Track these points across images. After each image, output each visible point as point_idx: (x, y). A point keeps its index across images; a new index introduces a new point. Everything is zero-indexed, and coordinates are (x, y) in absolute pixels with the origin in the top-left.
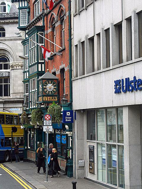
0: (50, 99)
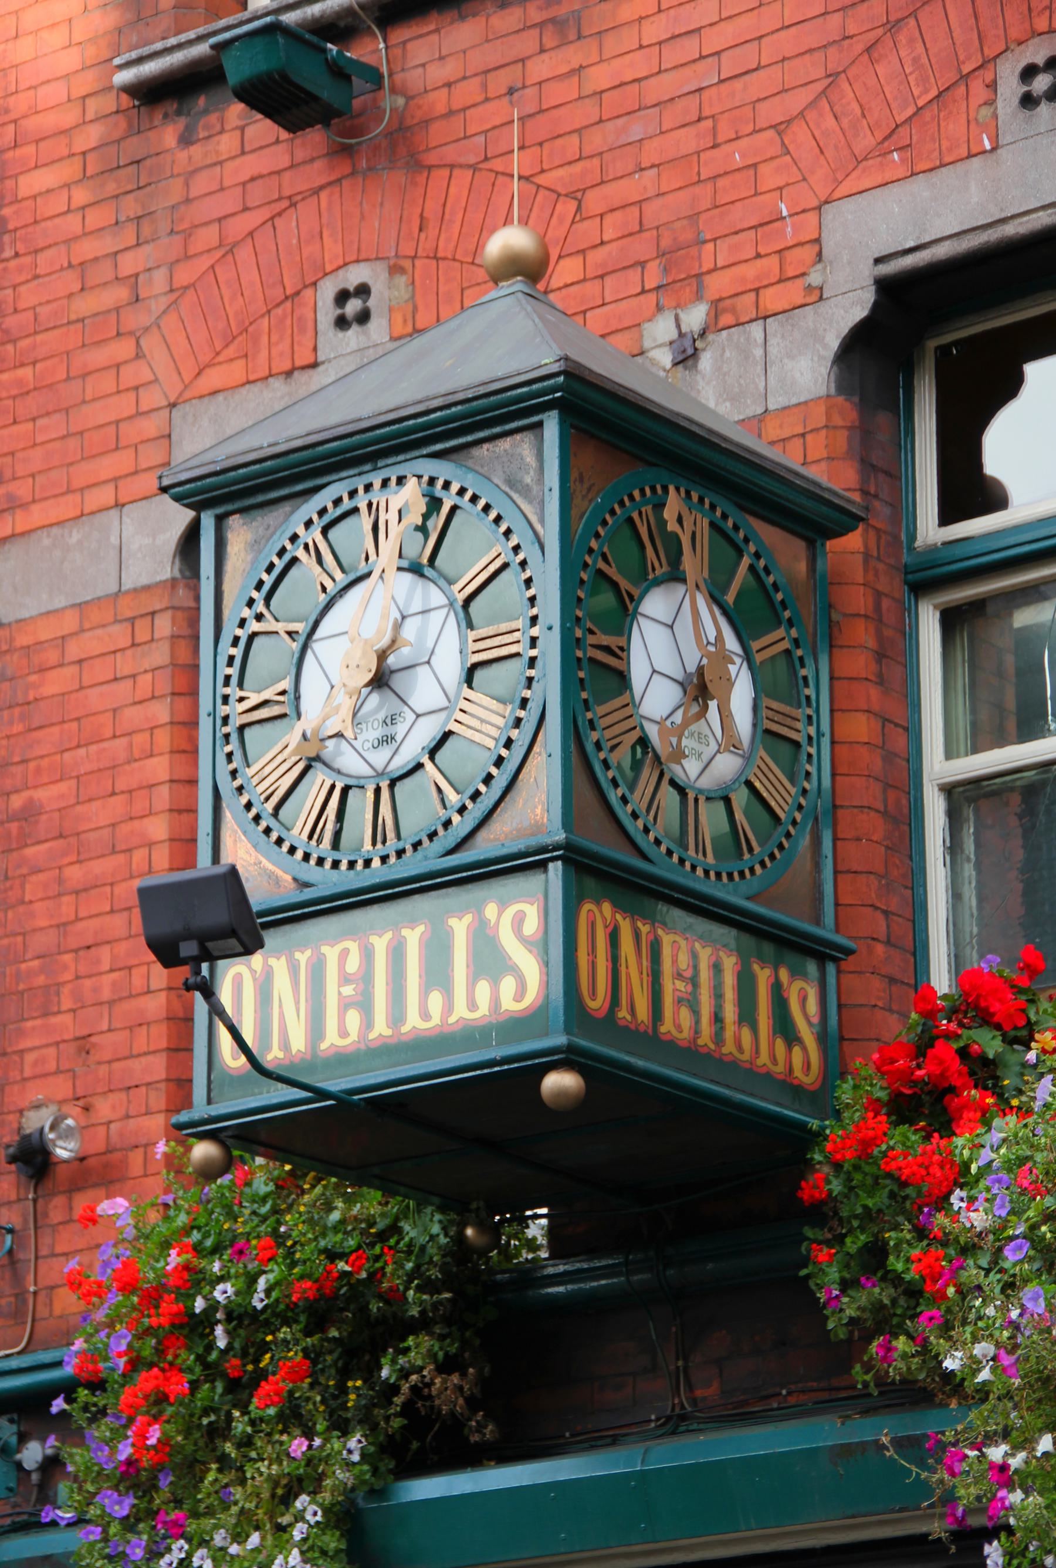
0: (365, 1006)
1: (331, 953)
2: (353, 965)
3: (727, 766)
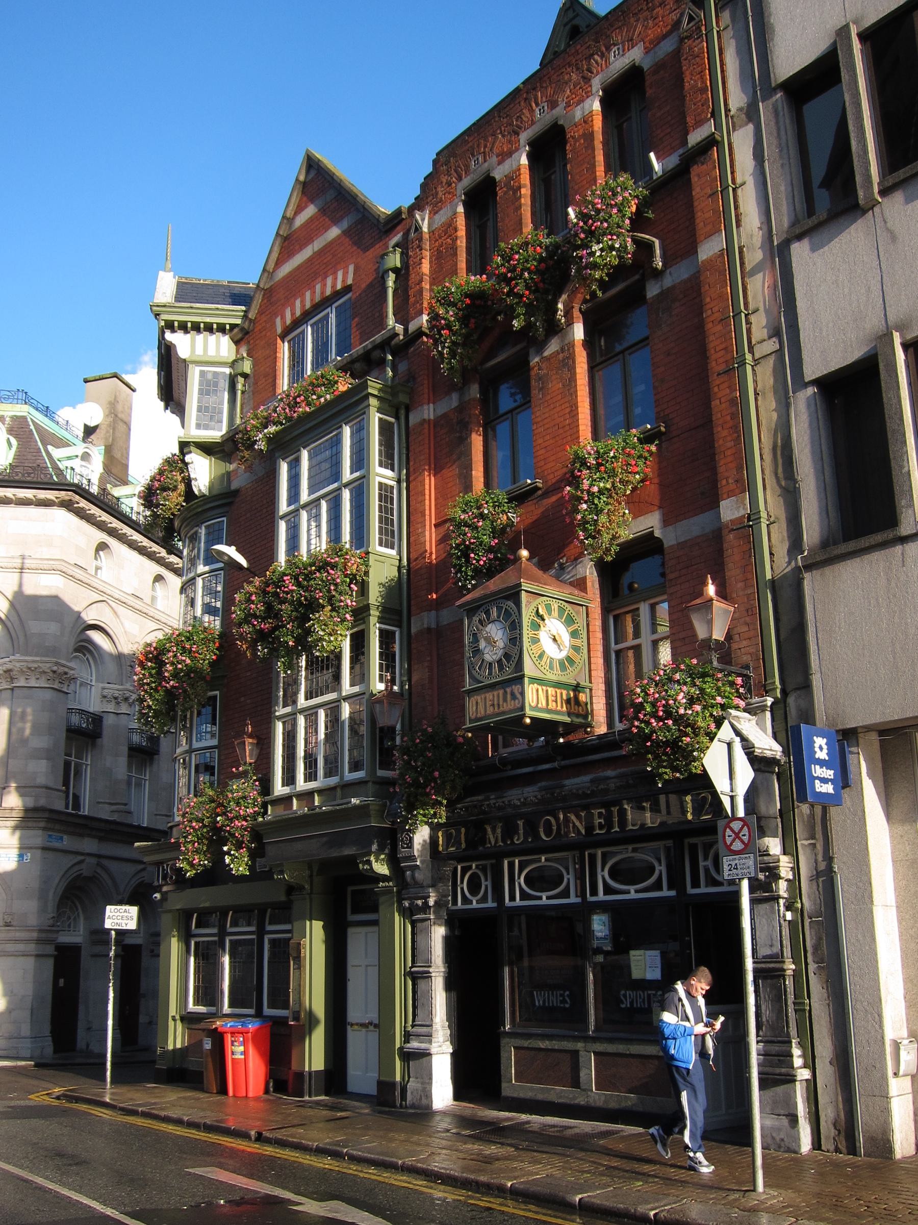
0: (556, 701)
1: (487, 695)
2: (554, 693)
3: (563, 655)
